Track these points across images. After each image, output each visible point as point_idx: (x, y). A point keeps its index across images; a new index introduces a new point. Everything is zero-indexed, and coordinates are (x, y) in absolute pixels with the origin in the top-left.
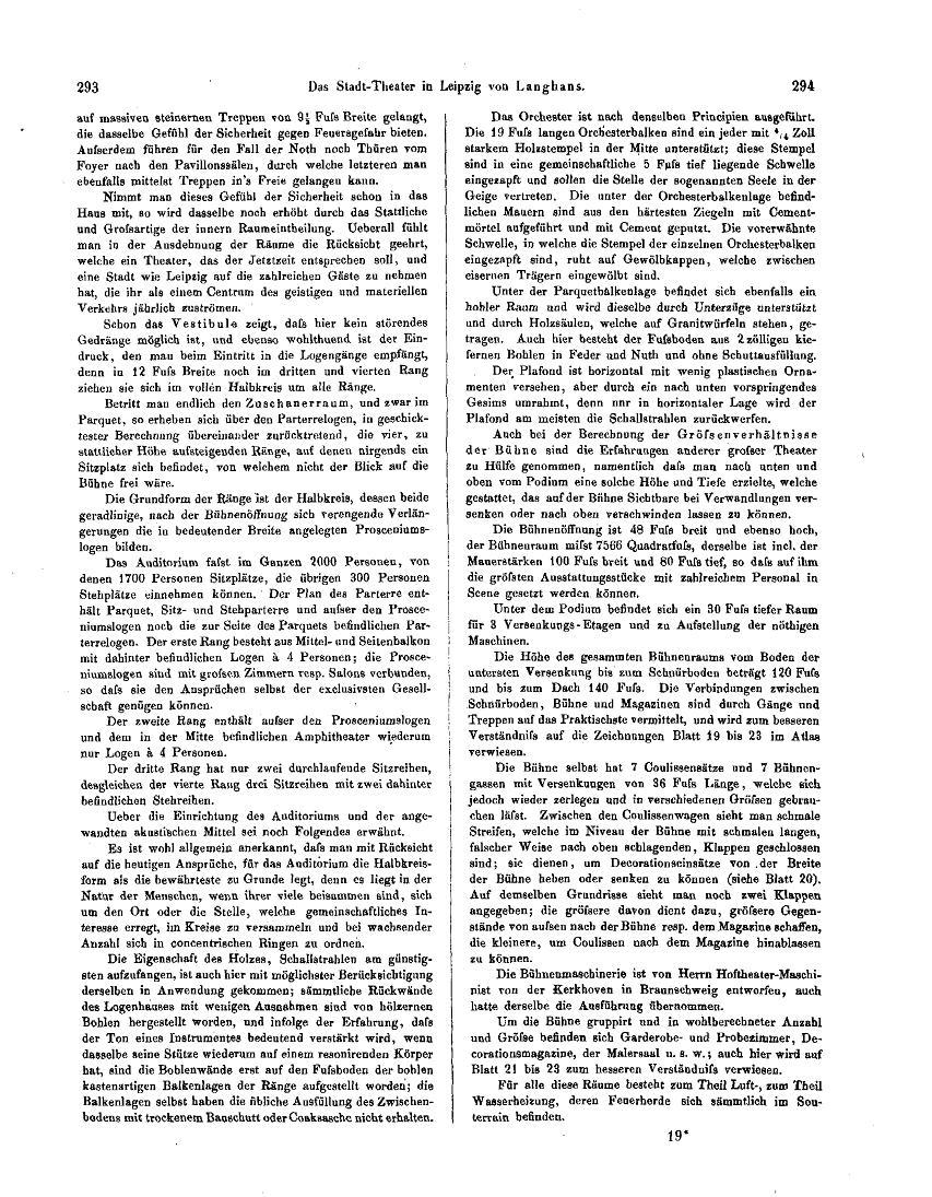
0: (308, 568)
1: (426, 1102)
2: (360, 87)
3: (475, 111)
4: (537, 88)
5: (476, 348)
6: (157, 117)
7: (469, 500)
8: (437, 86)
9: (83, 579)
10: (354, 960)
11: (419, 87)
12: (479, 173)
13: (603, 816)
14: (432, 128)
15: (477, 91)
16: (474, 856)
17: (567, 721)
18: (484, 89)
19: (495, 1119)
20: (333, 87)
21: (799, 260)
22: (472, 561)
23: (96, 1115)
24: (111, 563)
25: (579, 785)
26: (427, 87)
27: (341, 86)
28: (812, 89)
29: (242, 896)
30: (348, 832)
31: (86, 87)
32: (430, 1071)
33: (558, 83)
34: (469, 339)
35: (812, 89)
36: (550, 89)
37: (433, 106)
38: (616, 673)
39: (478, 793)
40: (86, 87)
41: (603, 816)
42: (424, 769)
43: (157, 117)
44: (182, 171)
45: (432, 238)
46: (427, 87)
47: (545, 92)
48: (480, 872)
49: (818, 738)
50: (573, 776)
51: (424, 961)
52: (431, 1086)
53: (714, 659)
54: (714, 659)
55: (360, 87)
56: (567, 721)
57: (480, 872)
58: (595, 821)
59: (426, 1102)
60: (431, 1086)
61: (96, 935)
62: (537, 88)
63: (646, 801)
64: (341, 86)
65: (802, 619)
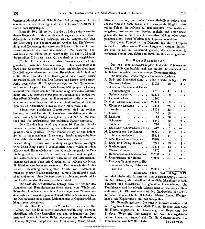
0: (170, 22)
2: (106, 13)
6: (59, 25)
9: (105, 69)
11: (127, 13)
13: (83, 165)
19: (133, 80)
24: (112, 65)
25: (124, 99)
26: (129, 13)
28: (95, 21)
31: (16, 13)
35: (95, 21)
40: (16, 13)
41: (83, 165)
43: (59, 25)
46: (129, 13)
53: (82, 206)
54: (82, 206)
55: (106, 13)
58: (81, 167)
64: (102, 13)
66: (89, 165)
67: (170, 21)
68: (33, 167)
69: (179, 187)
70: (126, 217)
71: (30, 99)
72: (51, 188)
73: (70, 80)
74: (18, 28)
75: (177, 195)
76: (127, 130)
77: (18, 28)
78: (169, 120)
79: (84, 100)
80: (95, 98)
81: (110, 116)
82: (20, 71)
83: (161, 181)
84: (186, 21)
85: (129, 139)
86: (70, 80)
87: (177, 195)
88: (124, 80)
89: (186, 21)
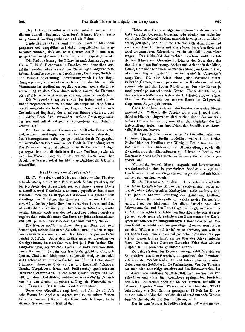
1: (112, 74)
3: (128, 28)
4: (145, 22)
5: (128, 58)
7: (125, 217)
8: (117, 22)
11: (112, 22)
12: (129, 54)
14: (116, 33)
15: (129, 23)
16: (126, 37)
18: (131, 22)
20: (89, 22)
21: (216, 100)
27: (91, 22)
34: (126, 56)
37: (117, 27)
38: (164, 96)
39: (127, 219)
42: (113, 130)
45: (116, 206)
47: (147, 23)
48: (128, 93)
49: (220, 243)
57: (128, 93)
59: (112, 74)
60: (113, 299)
61: (22, 123)
62: (145, 22)
64: (91, 22)
65: (214, 169)
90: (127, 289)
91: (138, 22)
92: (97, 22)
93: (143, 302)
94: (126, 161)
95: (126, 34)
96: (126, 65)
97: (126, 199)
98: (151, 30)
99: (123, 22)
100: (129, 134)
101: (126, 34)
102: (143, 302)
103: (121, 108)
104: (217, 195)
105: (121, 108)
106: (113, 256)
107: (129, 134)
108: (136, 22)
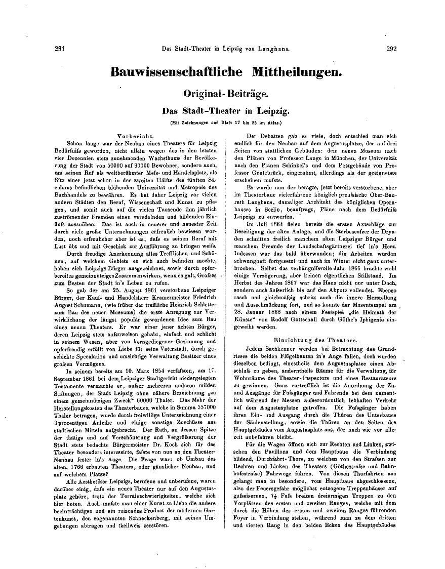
4: (268, 50)
7: (235, 482)
10: (200, 232)
17: (93, 475)
22: (236, 415)
23: (323, 252)
26: (217, 49)
29: (96, 203)
30: (261, 283)
32: (214, 386)
33: (278, 48)
36: (274, 50)
44: (256, 278)
46: (217, 49)
50: (348, 140)
51: (215, 145)
52: (395, 423)
56: (93, 475)
62: (268, 50)
63: (352, 188)
66: (311, 203)
67: (151, 371)
68: (145, 412)
69: (109, 156)
70: (235, 290)
71: (153, 504)
72: (68, 497)
73: (201, 253)
74: (284, 291)
75: (88, 296)
76: (370, 229)
77: (284, 291)
78: (73, 466)
79: (336, 381)
80: (111, 283)
81: (86, 266)
82: (255, 273)
83: (166, 305)
84: (395, 136)
85: (172, 217)
86: (201, 253)
87: (88, 296)
88: (100, 393)
89: (395, 136)
90: (238, 470)
91: (256, 49)
92: (186, 49)
93: (299, 140)
94: (235, 328)
95: (236, 230)
96: (236, 422)
97: (236, 282)
98: (264, 349)
99: (232, 50)
100: (240, 445)
101: (236, 230)
102: (299, 140)
103: (227, 445)
104: (392, 298)
105: (227, 445)
106: (214, 496)
107: (240, 445)
108: (253, 49)
